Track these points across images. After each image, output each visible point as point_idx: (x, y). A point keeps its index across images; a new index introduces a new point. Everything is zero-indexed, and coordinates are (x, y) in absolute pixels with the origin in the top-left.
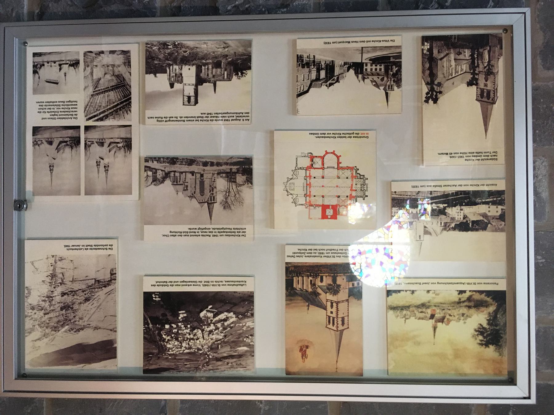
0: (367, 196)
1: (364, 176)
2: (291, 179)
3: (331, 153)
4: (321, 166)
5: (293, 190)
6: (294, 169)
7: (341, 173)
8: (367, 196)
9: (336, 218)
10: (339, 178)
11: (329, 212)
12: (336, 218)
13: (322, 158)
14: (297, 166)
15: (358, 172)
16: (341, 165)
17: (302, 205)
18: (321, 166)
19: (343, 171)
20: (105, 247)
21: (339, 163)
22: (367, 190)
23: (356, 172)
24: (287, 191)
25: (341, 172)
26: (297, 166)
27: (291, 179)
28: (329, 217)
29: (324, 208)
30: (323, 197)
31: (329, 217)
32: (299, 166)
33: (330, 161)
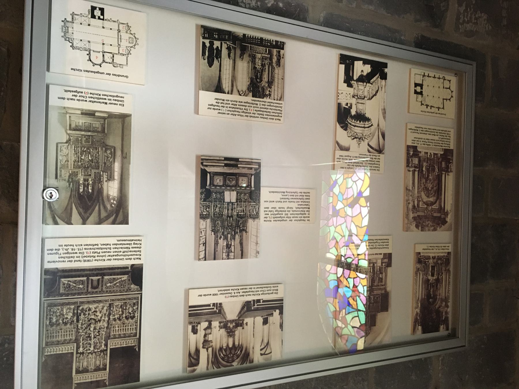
0: (65, 19)
1: (66, 40)
2: (132, 47)
3: (96, 64)
4: (105, 54)
5: (130, 38)
6: (129, 55)
7: (87, 45)
8: (65, 19)
9: (415, 93)
10: (89, 42)
11: (418, 89)
12: (415, 93)
13: (104, 61)
14: (127, 58)
15: (71, 44)
16: (88, 53)
17: (122, 24)
18: (105, 54)
19: (85, 46)
20: (109, 246)
21: (89, 54)
22: (62, 26)
23: (73, 44)
24: (135, 38)
25: (87, 47)
26: (127, 58)
27: (132, 47)
28: (98, 9)
29: (421, 86)
30: (103, 28)
31: (98, 9)
32: (125, 57)
33: (97, 58)
